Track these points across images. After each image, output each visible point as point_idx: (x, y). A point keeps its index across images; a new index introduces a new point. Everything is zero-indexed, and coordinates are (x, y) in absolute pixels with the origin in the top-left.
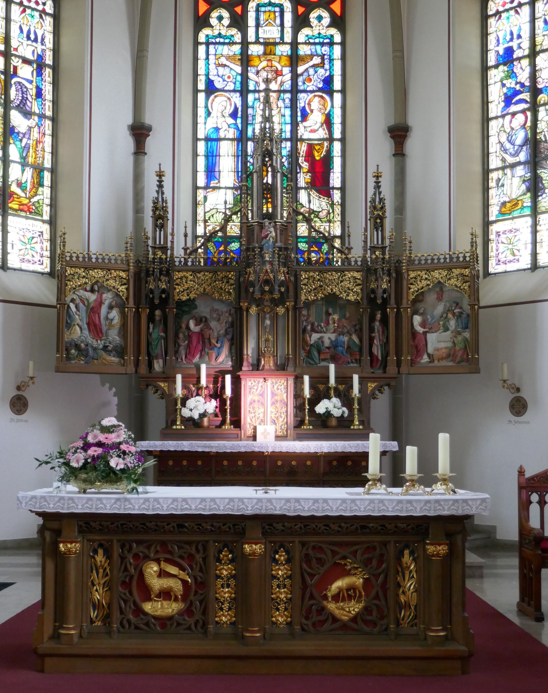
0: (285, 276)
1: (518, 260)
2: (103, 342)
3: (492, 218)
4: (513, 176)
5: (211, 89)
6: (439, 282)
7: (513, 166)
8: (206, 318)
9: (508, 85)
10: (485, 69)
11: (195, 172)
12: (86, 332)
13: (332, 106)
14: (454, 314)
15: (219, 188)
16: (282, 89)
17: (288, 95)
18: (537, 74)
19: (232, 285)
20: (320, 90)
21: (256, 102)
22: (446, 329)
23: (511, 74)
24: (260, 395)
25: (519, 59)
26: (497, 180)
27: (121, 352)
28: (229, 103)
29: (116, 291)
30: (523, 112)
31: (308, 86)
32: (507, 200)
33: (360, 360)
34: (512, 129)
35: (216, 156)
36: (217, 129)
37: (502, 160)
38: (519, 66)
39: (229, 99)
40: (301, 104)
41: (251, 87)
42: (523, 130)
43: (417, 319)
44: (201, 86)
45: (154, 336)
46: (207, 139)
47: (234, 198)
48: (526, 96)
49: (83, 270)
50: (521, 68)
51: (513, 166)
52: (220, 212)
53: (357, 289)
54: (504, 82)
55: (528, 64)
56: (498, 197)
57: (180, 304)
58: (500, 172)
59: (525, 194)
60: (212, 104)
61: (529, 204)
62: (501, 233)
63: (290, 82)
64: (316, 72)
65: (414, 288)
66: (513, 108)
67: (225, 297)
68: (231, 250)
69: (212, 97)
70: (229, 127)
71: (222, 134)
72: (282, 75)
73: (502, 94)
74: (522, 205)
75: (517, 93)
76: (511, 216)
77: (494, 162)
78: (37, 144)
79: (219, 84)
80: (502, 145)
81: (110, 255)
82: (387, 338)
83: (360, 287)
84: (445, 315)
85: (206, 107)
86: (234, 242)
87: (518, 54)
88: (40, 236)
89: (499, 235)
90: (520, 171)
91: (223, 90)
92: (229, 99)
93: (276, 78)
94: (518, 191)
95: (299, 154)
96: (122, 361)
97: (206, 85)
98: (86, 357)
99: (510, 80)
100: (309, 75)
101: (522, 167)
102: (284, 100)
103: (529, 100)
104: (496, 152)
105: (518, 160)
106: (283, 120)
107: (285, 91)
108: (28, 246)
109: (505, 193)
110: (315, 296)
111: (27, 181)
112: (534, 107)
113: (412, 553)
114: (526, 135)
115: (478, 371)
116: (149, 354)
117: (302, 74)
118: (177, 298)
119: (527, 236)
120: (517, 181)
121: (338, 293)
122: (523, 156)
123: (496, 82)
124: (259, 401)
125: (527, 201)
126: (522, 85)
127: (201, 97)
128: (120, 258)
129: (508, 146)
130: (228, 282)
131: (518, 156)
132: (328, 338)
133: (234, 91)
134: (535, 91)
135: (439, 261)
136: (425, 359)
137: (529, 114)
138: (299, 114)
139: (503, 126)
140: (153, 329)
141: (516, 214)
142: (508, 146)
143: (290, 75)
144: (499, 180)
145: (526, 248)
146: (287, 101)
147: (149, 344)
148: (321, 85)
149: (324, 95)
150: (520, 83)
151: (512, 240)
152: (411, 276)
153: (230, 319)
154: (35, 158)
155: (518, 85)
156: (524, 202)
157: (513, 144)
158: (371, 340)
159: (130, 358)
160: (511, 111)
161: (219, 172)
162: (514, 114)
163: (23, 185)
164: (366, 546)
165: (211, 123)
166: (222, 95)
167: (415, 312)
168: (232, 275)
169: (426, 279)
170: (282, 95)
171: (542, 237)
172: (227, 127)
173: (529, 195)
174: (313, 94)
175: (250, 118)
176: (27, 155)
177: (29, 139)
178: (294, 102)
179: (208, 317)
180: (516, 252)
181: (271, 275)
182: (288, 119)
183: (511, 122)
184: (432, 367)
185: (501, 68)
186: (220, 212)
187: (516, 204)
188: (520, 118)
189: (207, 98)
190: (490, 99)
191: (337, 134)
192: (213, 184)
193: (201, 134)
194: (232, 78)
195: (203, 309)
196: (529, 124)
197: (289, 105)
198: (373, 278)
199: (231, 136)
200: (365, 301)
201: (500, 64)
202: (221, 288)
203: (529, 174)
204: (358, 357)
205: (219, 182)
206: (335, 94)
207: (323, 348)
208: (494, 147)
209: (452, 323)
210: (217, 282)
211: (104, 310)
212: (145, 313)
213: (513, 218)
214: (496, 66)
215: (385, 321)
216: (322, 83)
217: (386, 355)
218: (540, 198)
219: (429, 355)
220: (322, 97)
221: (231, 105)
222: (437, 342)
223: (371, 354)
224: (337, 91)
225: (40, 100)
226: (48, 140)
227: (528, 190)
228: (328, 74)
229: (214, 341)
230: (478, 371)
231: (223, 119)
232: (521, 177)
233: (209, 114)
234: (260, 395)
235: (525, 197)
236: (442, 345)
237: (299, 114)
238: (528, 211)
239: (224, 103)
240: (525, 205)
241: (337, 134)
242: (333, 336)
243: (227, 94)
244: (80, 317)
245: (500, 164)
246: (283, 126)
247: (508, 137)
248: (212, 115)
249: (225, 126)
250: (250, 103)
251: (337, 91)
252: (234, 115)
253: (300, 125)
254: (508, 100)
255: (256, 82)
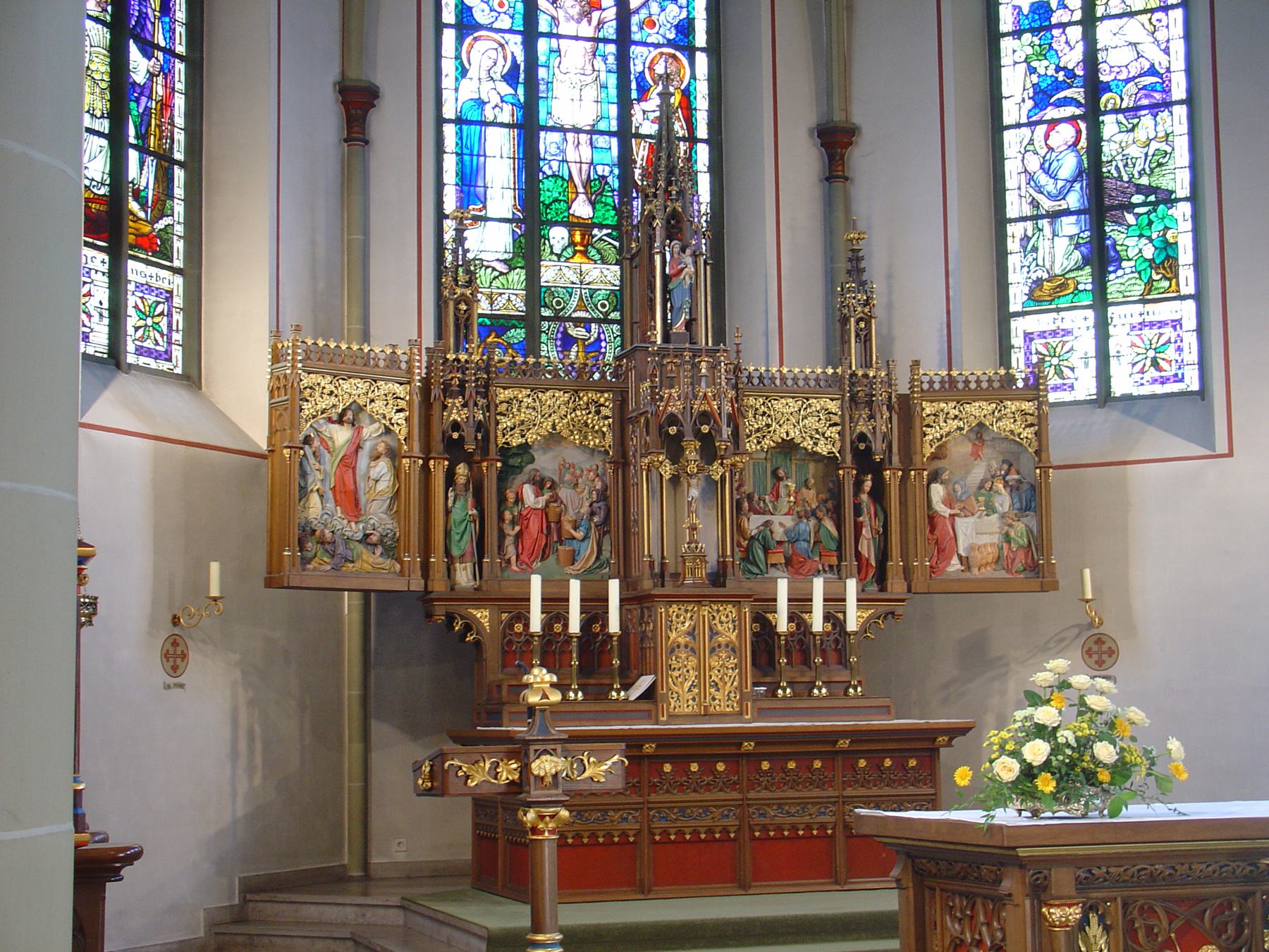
0: (733, 406)
1: (1072, 387)
2: (361, 526)
3: (1013, 308)
4: (1054, 234)
5: (466, 25)
6: (981, 425)
7: (1054, 216)
8: (553, 482)
9: (1041, 71)
10: (993, 37)
11: (440, 185)
12: (330, 505)
13: (693, 77)
14: (1006, 484)
15: (486, 219)
16: (601, 35)
17: (612, 48)
18: (1099, 56)
19: (607, 418)
20: (670, 43)
21: (554, 55)
22: (990, 509)
23: (1045, 51)
24: (689, 634)
25: (1063, 26)
26: (1022, 240)
27: (391, 548)
28: (501, 55)
29: (388, 423)
30: (1072, 120)
31: (649, 35)
32: (1046, 276)
33: (839, 566)
34: (1051, 149)
35: (478, 155)
36: (481, 103)
37: (1031, 203)
38: (1063, 39)
39: (502, 45)
40: (636, 67)
41: (543, 26)
42: (1074, 154)
43: (938, 491)
44: (449, 16)
45: (457, 515)
46: (460, 121)
47: (514, 241)
48: (1077, 93)
49: (329, 378)
50: (1067, 42)
51: (1054, 216)
52: (487, 267)
53: (833, 432)
54: (1034, 64)
55: (1080, 37)
56: (1026, 269)
57: (505, 451)
58: (1029, 224)
59: (1079, 268)
60: (469, 53)
61: (1089, 287)
62: (1035, 336)
63: (614, 23)
64: (663, 10)
65: (932, 433)
66: (1051, 113)
67: (593, 442)
68: (509, 344)
69: (469, 40)
70: (502, 101)
71: (489, 114)
72: (600, 8)
73: (1029, 85)
74: (1076, 288)
75: (1058, 86)
76: (1053, 307)
77: (1015, 206)
78: (162, 109)
79: (481, 16)
80: (1031, 178)
81: (932, 373)
82: (886, 526)
83: (839, 428)
84: (988, 485)
85: (458, 57)
86: (515, 327)
87: (1059, 16)
88: (167, 299)
89: (1031, 340)
90: (1069, 226)
91: (490, 28)
92: (502, 45)
93: (590, 13)
94: (1066, 263)
95: (635, 162)
96: (398, 567)
97: (457, 16)
98: (333, 556)
99: (1045, 63)
100: (650, 15)
101: (1073, 219)
102: (605, 58)
103: (1083, 101)
104: (1019, 188)
105: (1065, 206)
106: (603, 95)
107: (606, 41)
108: (149, 322)
109: (1040, 263)
110: (759, 443)
111: (147, 187)
112: (1092, 114)
113: (1101, 920)
114: (1080, 162)
115: (1054, 586)
116: (448, 553)
117: (637, 11)
118: (501, 441)
119: (1085, 343)
120: (1062, 244)
121: (798, 440)
122: (1074, 200)
123: (1016, 63)
124: (686, 646)
125: (1085, 278)
126: (1070, 74)
127: (449, 36)
128: (814, 376)
129: (1043, 179)
130: (598, 412)
131: (1064, 198)
132: (782, 523)
133: (511, 31)
134: (1095, 88)
135: (931, 387)
136: (955, 565)
137: (1083, 126)
138: (634, 85)
139: (1031, 142)
140: (454, 502)
141: (1063, 302)
142: (1043, 179)
143: (614, 9)
144: (1026, 239)
145: (1086, 365)
146: (611, 59)
147: (447, 533)
148: (672, 36)
149: (678, 54)
150: (1065, 69)
151: (1058, 350)
152: (928, 411)
153: (599, 485)
154: (160, 139)
155: (1062, 73)
156: (1078, 283)
157: (1055, 178)
158: (858, 528)
159: (412, 559)
160: (1047, 118)
161: (485, 187)
162: (1053, 123)
163: (143, 194)
164: (1218, 902)
165: (468, 89)
166: (488, 38)
167: (935, 477)
168: (606, 400)
169: (956, 417)
170: (601, 45)
171: (1118, 348)
172: (499, 100)
173: (1088, 269)
174: (659, 50)
175: (542, 87)
176: (147, 131)
177: (150, 98)
178: (623, 60)
179: (556, 479)
180: (1067, 372)
181: (715, 405)
182: (613, 92)
183: (1047, 137)
184: (966, 580)
185: (1027, 37)
186: (487, 267)
187: (1063, 286)
188: (1065, 133)
189: (460, 40)
190: (1006, 91)
191: (702, 132)
192: (474, 209)
193: (449, 112)
194: (506, 7)
195: (545, 463)
196: (1083, 143)
197: (614, 67)
198: (865, 413)
199: (505, 117)
200: (849, 458)
201: (1025, 31)
202: (586, 425)
203: (1088, 233)
204: (834, 561)
205: (485, 207)
206: (698, 54)
207: (773, 544)
208: (1012, 179)
209: (1004, 501)
210: (578, 413)
211: (363, 461)
212: (439, 469)
213: (1058, 310)
214: (1017, 34)
215: (879, 494)
216: (674, 32)
217: (883, 555)
218: (1112, 276)
219: (960, 557)
220: (674, 57)
221: (505, 58)
222: (978, 533)
223: (858, 555)
224: (449, 26)
225: (167, 20)
226: (179, 102)
227: (1086, 261)
228: (684, 15)
229: (567, 527)
230: (1054, 586)
231: (491, 84)
232: (1071, 237)
233: (464, 72)
234: (689, 634)
235: (1081, 273)
236: (985, 539)
237: (634, 85)
238: (1087, 299)
239: (493, 54)
240: (1081, 287)
241: (702, 132)
242: (789, 522)
243: (497, 36)
244: (322, 474)
245: (1027, 210)
246: (605, 106)
247: (1042, 165)
248: (469, 75)
249: (495, 99)
250: (542, 59)
251: (449, 26)
252: (511, 77)
253: (636, 106)
254: (1042, 97)
255: (553, 18)
